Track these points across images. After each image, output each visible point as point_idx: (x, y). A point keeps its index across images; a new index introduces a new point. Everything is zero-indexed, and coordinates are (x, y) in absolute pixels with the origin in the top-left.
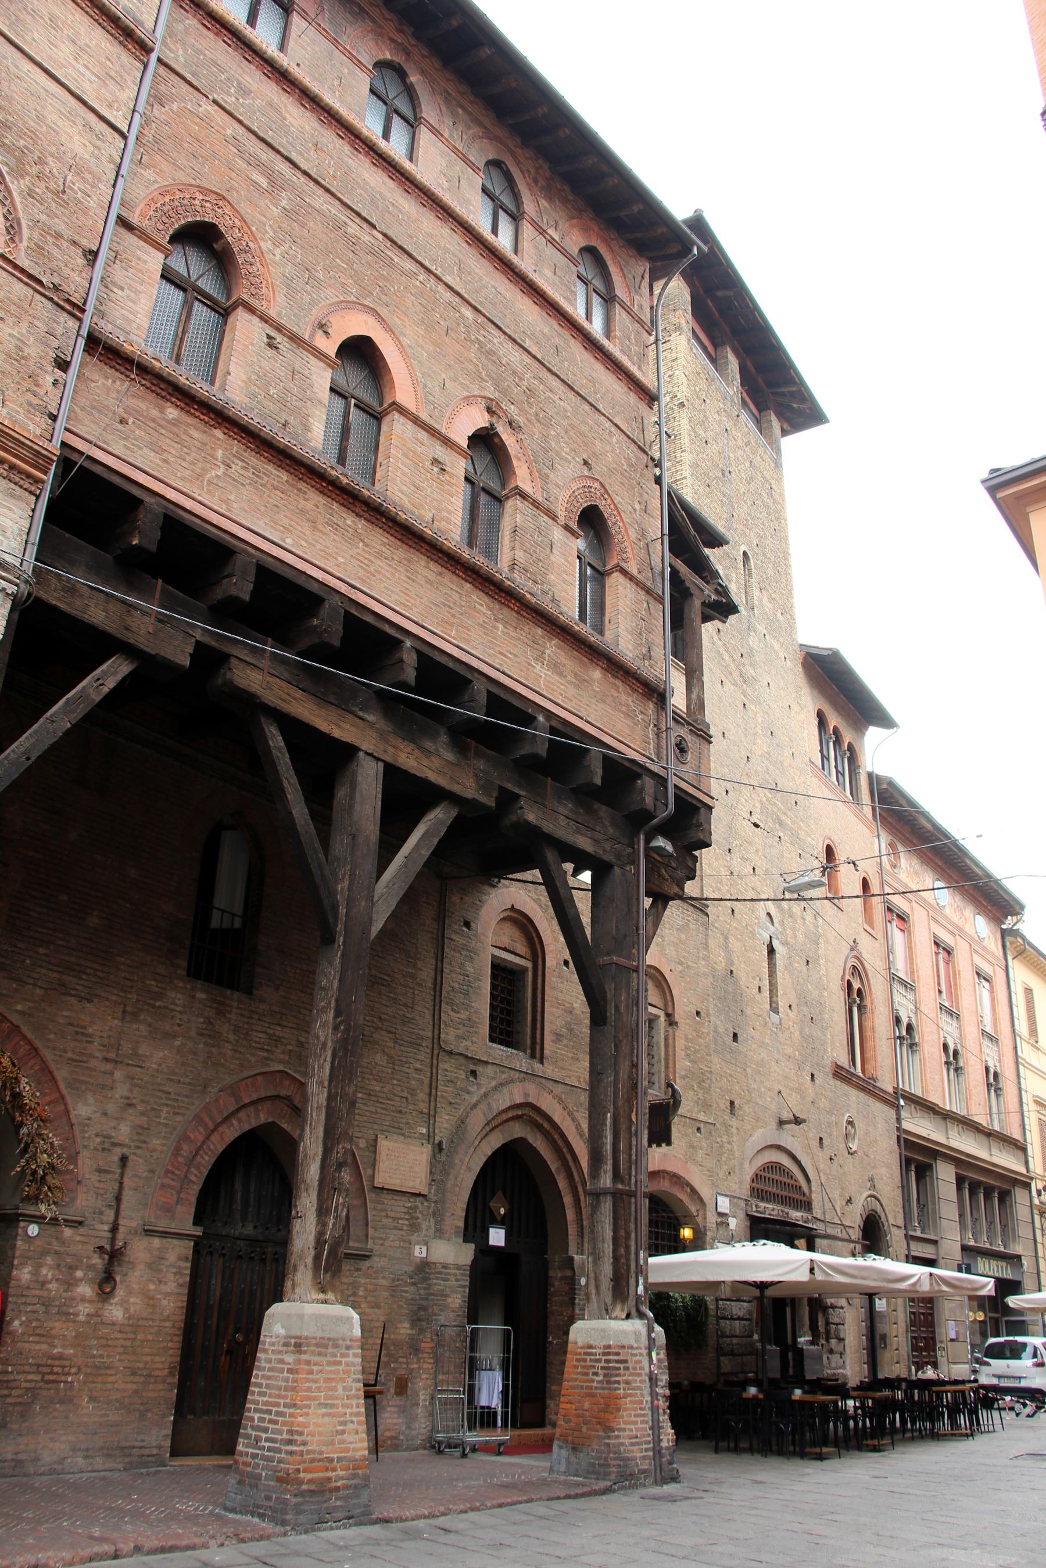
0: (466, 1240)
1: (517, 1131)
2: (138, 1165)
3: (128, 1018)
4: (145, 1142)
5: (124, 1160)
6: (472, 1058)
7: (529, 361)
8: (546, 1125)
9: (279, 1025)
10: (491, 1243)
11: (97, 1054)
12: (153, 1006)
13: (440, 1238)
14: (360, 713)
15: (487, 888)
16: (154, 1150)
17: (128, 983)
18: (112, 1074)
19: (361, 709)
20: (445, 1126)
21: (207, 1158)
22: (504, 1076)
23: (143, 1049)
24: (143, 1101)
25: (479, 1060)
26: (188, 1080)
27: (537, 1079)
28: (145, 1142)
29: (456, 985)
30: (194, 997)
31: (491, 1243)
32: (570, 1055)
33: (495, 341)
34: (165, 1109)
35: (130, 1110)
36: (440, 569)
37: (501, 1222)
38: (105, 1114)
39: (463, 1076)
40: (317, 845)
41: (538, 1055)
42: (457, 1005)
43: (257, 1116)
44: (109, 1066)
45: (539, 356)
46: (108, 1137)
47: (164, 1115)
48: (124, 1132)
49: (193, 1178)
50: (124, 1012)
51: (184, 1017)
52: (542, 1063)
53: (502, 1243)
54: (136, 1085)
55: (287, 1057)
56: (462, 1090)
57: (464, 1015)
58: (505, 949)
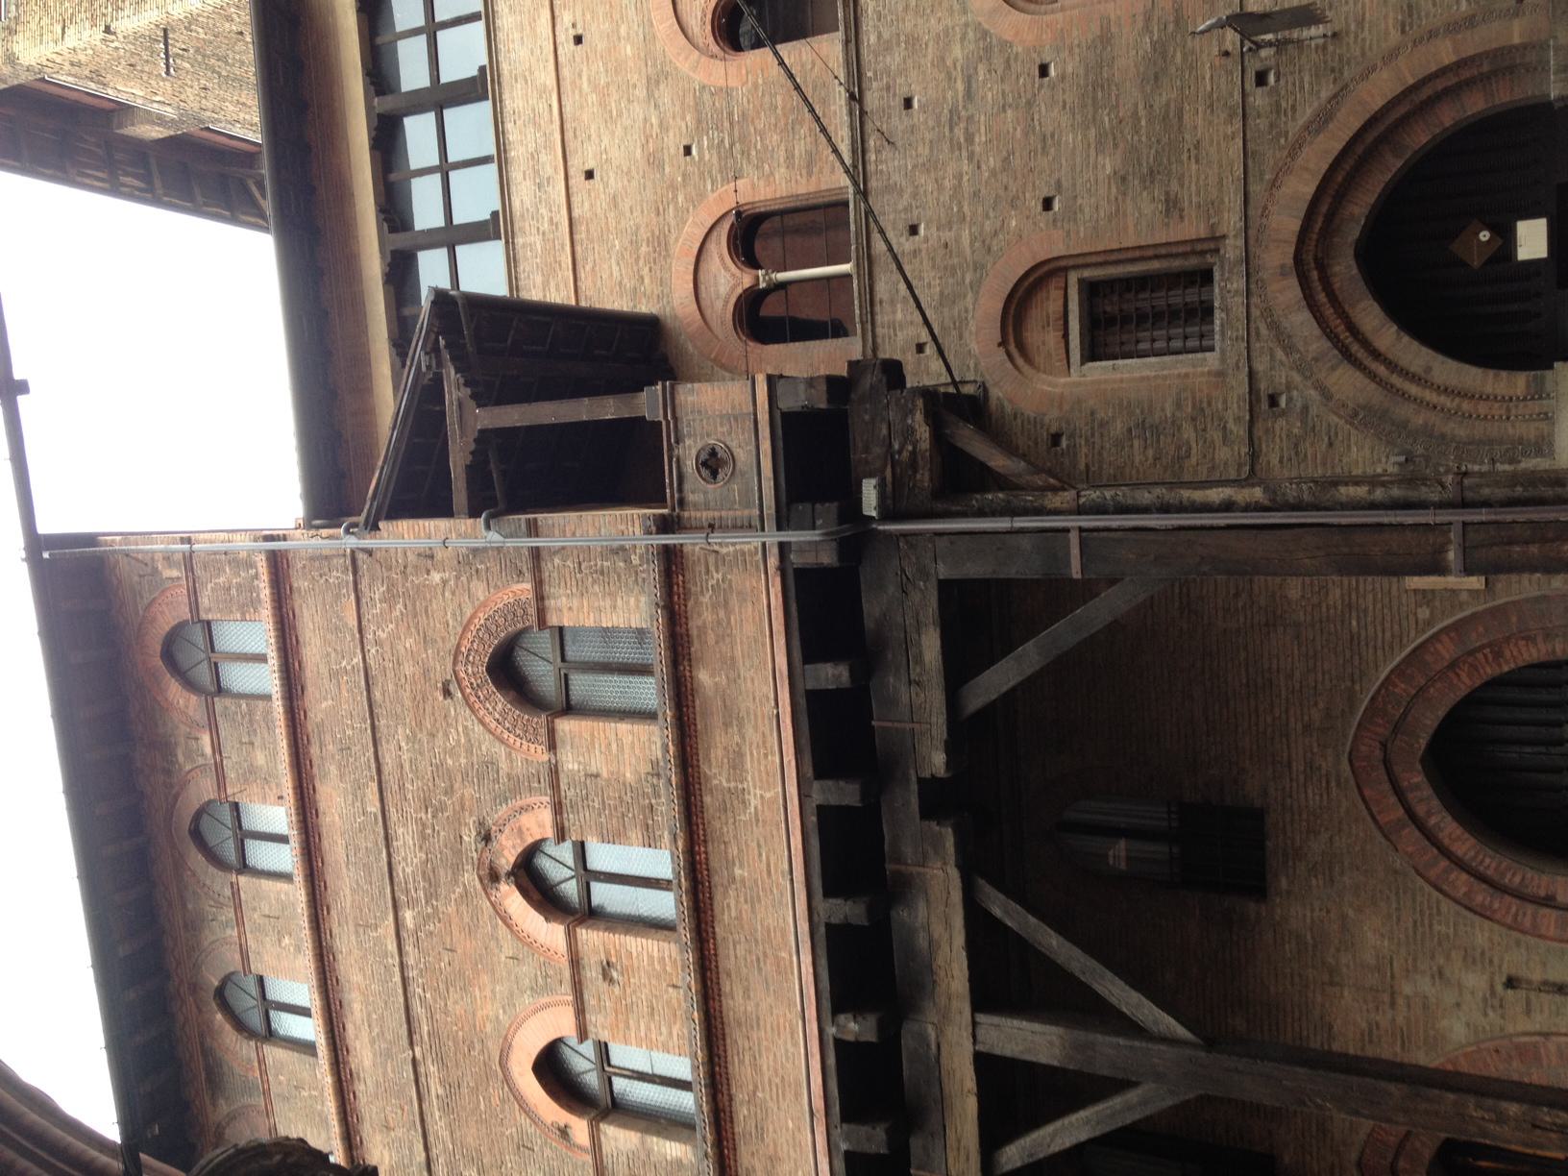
0: (1551, 367)
1: (1345, 269)
2: (1514, 960)
3: (1337, 979)
4: (1483, 953)
5: (1511, 983)
6: (1251, 411)
7: (393, 810)
8: (1324, 208)
9: (1290, 767)
10: (1544, 255)
11: (1389, 1016)
12: (1315, 946)
13: (1551, 444)
14: (933, 1047)
15: (993, 403)
16: (1491, 940)
17: (1297, 979)
18: (1407, 997)
19: (928, 1046)
20: (1367, 452)
21: (1487, 861)
22: (1264, 331)
23: (1369, 958)
24: (1433, 957)
25: (1250, 392)
26: (1393, 898)
27: (1252, 249)
28: (1483, 953)
29: (1150, 452)
30: (1289, 892)
31: (1544, 255)
32: (1194, 167)
33: (409, 870)
34: (1436, 927)
35: (1447, 973)
36: (723, 976)
37: (1507, 238)
38: (1458, 1005)
39: (1281, 422)
40: (1117, 1102)
41: (1212, 246)
42: (1179, 448)
43: (1417, 787)
44: (1400, 1001)
45: (374, 786)
46: (1485, 1000)
47: (1443, 929)
48: (1475, 981)
49: (1517, 879)
50: (1332, 984)
51: (1317, 904)
52: (1224, 237)
53: (1541, 225)
54: (1415, 967)
55: (1329, 751)
56: (1304, 422)
57: (1188, 433)
58: (1066, 336)
